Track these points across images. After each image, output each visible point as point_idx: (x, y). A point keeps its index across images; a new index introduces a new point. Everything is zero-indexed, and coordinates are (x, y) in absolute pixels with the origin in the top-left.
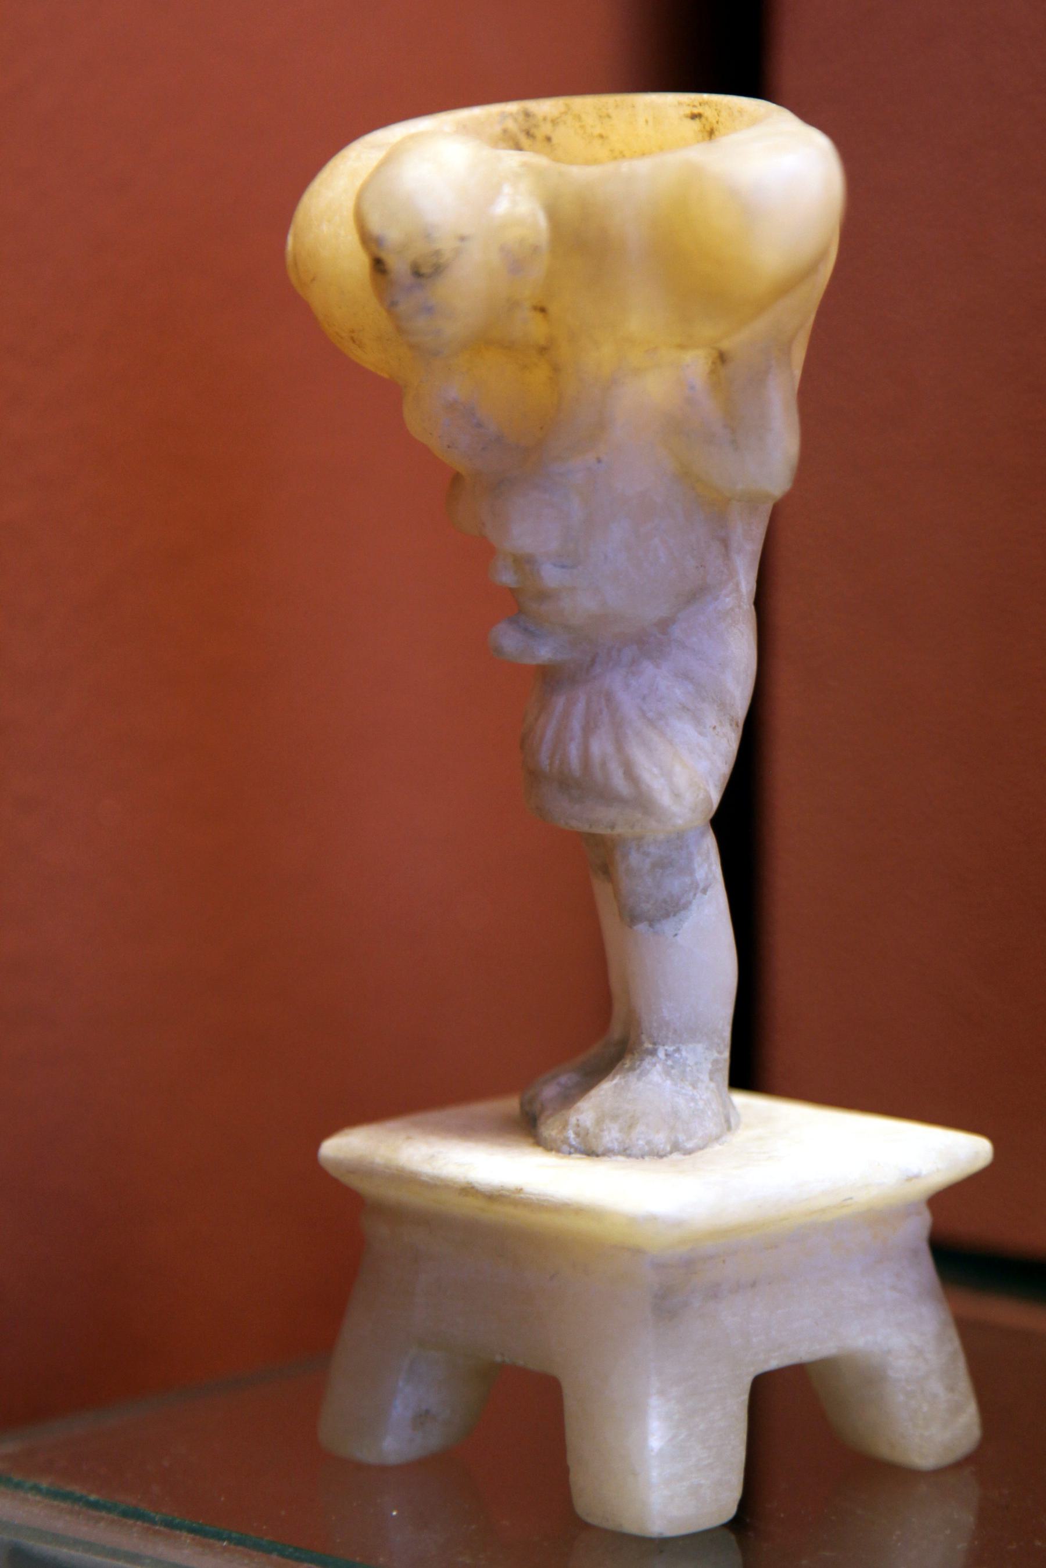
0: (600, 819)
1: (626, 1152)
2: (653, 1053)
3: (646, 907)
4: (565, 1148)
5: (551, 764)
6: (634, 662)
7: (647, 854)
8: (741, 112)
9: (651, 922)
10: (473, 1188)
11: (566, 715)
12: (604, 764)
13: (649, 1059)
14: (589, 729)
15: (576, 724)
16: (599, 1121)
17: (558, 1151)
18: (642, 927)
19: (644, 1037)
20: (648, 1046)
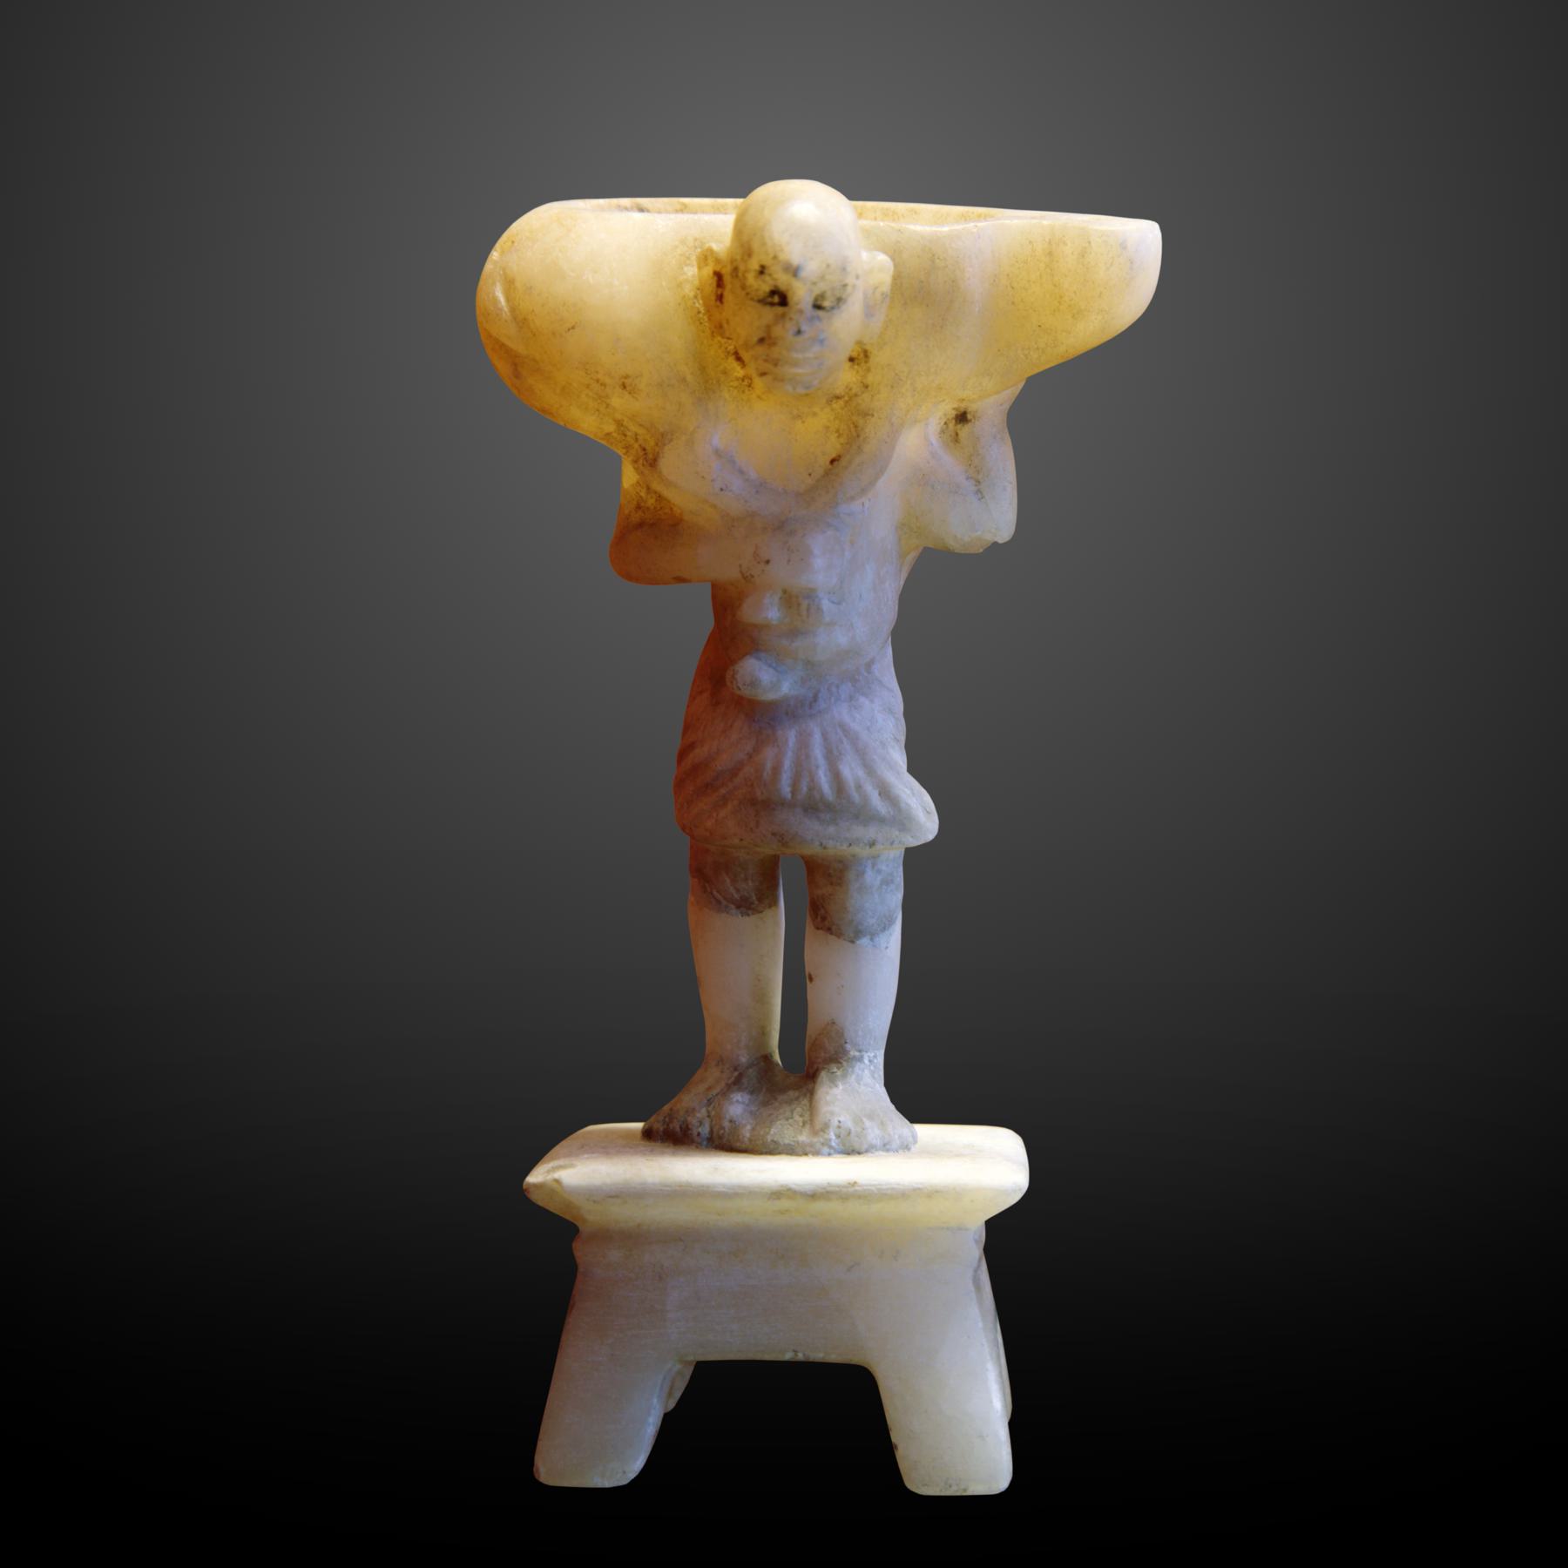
0: (821, 838)
1: (886, 1147)
2: (860, 1059)
3: (872, 921)
4: (826, 1150)
5: (793, 793)
6: (851, 698)
7: (879, 871)
8: (894, 213)
9: (873, 936)
10: (789, 1189)
11: (804, 744)
12: (859, 787)
13: (858, 1066)
14: (832, 759)
15: (818, 752)
16: (858, 1120)
17: (817, 1153)
18: (864, 941)
19: (848, 1046)
20: (853, 1053)
